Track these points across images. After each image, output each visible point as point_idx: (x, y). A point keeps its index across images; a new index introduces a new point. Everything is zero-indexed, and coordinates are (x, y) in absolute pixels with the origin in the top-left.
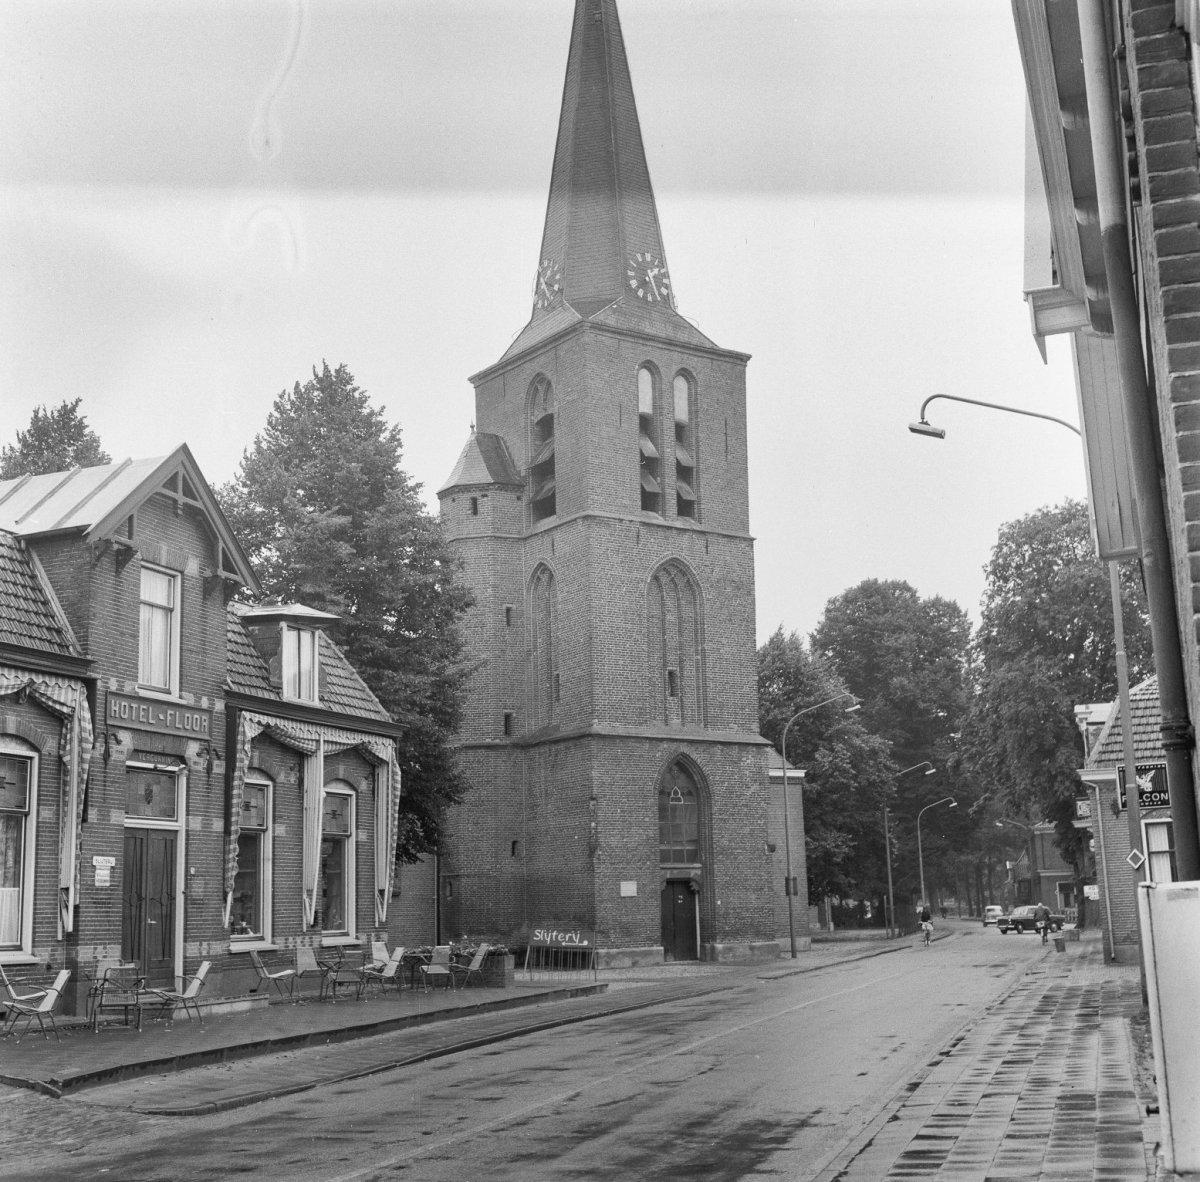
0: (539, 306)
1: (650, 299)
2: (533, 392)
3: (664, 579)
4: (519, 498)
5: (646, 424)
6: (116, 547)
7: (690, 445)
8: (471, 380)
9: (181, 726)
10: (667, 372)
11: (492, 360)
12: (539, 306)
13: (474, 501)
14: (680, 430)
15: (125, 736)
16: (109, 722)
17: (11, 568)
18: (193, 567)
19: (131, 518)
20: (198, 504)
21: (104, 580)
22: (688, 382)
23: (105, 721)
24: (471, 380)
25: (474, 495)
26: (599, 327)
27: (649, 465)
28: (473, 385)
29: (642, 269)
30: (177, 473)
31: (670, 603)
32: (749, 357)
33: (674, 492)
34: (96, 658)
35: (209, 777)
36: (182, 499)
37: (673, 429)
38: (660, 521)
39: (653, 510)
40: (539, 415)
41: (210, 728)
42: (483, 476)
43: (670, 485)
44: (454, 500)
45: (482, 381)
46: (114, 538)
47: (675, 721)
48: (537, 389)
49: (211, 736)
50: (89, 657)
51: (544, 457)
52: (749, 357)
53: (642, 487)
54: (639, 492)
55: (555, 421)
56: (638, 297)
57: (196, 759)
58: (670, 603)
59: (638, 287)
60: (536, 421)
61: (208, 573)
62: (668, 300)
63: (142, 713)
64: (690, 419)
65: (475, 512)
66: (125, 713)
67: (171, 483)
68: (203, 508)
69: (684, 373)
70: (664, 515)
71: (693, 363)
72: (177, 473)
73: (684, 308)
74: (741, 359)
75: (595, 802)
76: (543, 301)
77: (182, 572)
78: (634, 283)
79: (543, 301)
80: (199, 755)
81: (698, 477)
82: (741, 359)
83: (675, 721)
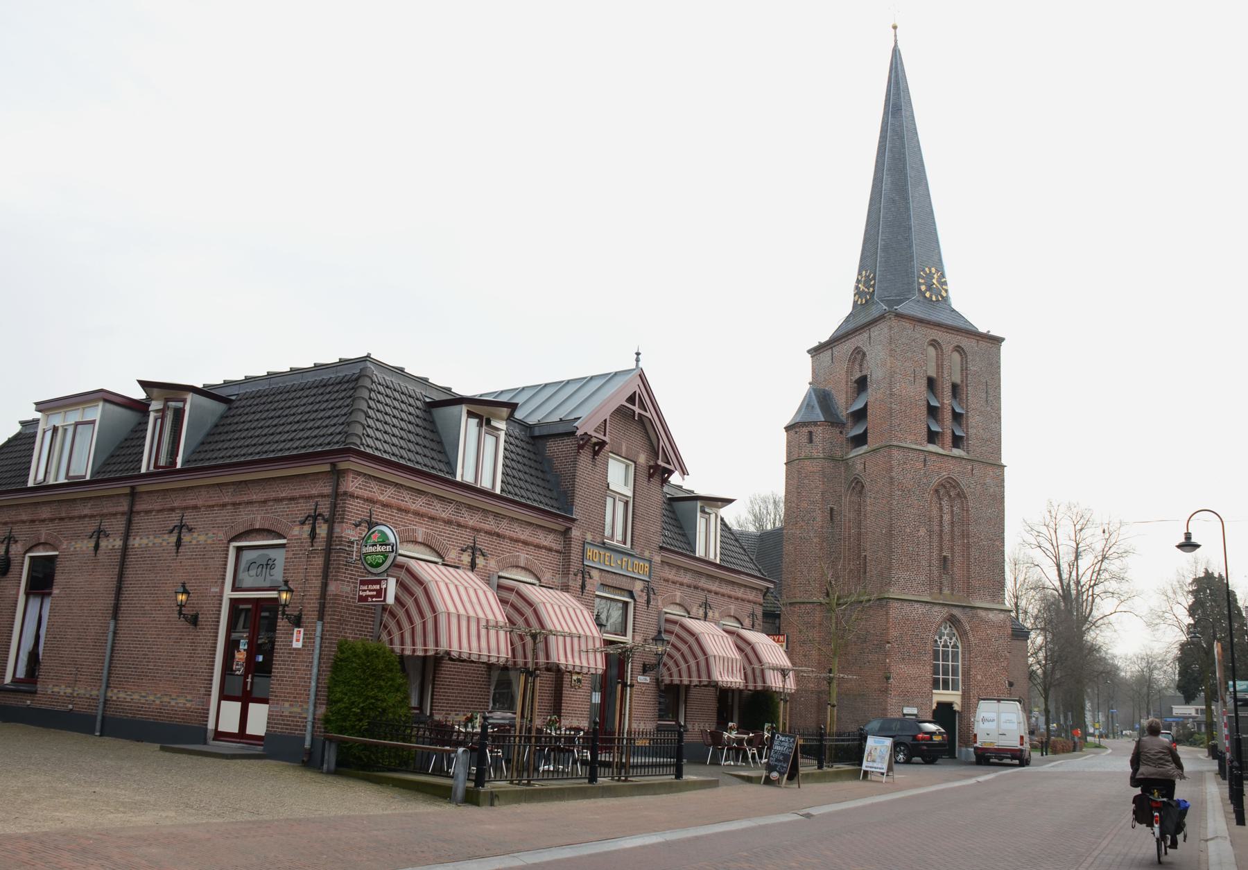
0: (859, 303)
1: (934, 299)
2: (852, 360)
3: (942, 492)
4: (841, 432)
5: (931, 383)
6: (594, 440)
7: (961, 399)
8: (809, 352)
9: (608, 564)
10: (947, 349)
11: (825, 338)
12: (859, 303)
13: (810, 433)
14: (955, 387)
15: (595, 574)
16: (585, 563)
17: (542, 477)
18: (642, 459)
19: (605, 420)
20: (648, 415)
21: (585, 457)
22: (961, 355)
23: (583, 562)
24: (809, 352)
25: (810, 429)
26: (899, 316)
27: (933, 412)
28: (810, 356)
29: (930, 276)
30: (635, 392)
31: (946, 509)
32: (1003, 339)
33: (950, 431)
34: (578, 517)
35: (648, 607)
36: (637, 409)
37: (950, 387)
38: (941, 451)
39: (934, 443)
40: (857, 375)
41: (650, 573)
42: (819, 416)
43: (946, 426)
44: (796, 433)
45: (816, 351)
46: (594, 434)
47: (946, 591)
48: (855, 358)
49: (650, 578)
50: (574, 517)
51: (858, 405)
52: (1003, 339)
53: (929, 428)
54: (926, 430)
55: (868, 380)
56: (926, 297)
57: (640, 593)
58: (946, 509)
59: (926, 290)
60: (854, 380)
61: (652, 463)
62: (946, 299)
63: (606, 559)
64: (962, 381)
65: (811, 441)
66: (596, 557)
67: (631, 399)
68: (650, 417)
69: (958, 349)
70: (943, 448)
71: (965, 343)
72: (635, 392)
73: (956, 304)
74: (997, 341)
75: (890, 645)
76: (862, 300)
77: (635, 463)
78: (923, 288)
79: (862, 300)
80: (642, 591)
81: (967, 420)
82: (997, 341)
83: (946, 591)
